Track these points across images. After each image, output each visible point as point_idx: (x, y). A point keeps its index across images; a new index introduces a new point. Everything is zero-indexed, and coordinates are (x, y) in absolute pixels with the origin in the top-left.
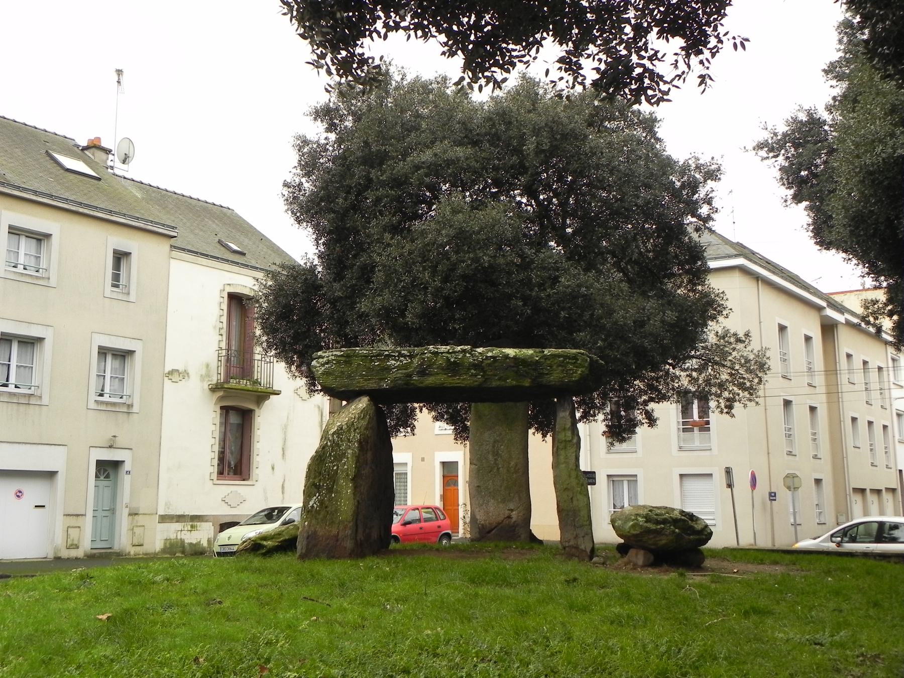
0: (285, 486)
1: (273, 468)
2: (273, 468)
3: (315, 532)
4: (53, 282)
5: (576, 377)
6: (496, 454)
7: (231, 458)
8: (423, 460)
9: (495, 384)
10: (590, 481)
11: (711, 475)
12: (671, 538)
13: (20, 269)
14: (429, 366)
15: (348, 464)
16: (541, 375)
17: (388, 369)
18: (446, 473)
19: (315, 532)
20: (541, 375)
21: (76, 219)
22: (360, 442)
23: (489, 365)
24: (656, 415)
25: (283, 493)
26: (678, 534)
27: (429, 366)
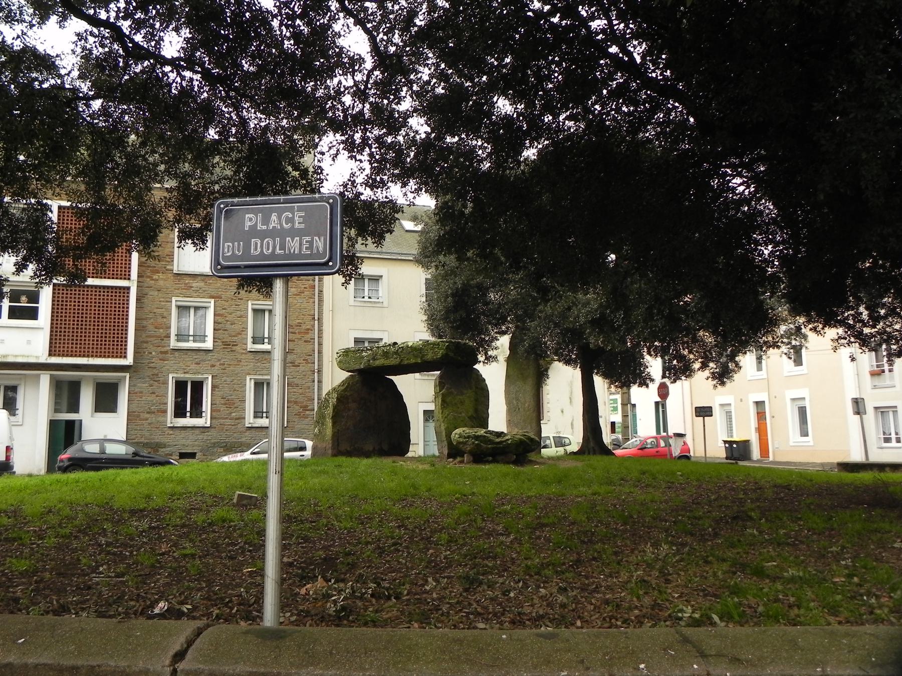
0: (574, 423)
1: (562, 412)
2: (562, 412)
3: (317, 446)
4: (385, 304)
5: (439, 355)
6: (517, 399)
7: (861, 405)
8: (741, 400)
9: (406, 362)
10: (708, 413)
11: (759, 404)
12: (472, 446)
13: (366, 299)
14: (376, 355)
15: (330, 411)
16: (423, 356)
17: (363, 357)
18: (759, 411)
19: (317, 446)
20: (423, 356)
21: (398, 264)
22: (337, 398)
23: (401, 352)
24: (741, 364)
25: (572, 428)
26: (478, 444)
27: (376, 355)
